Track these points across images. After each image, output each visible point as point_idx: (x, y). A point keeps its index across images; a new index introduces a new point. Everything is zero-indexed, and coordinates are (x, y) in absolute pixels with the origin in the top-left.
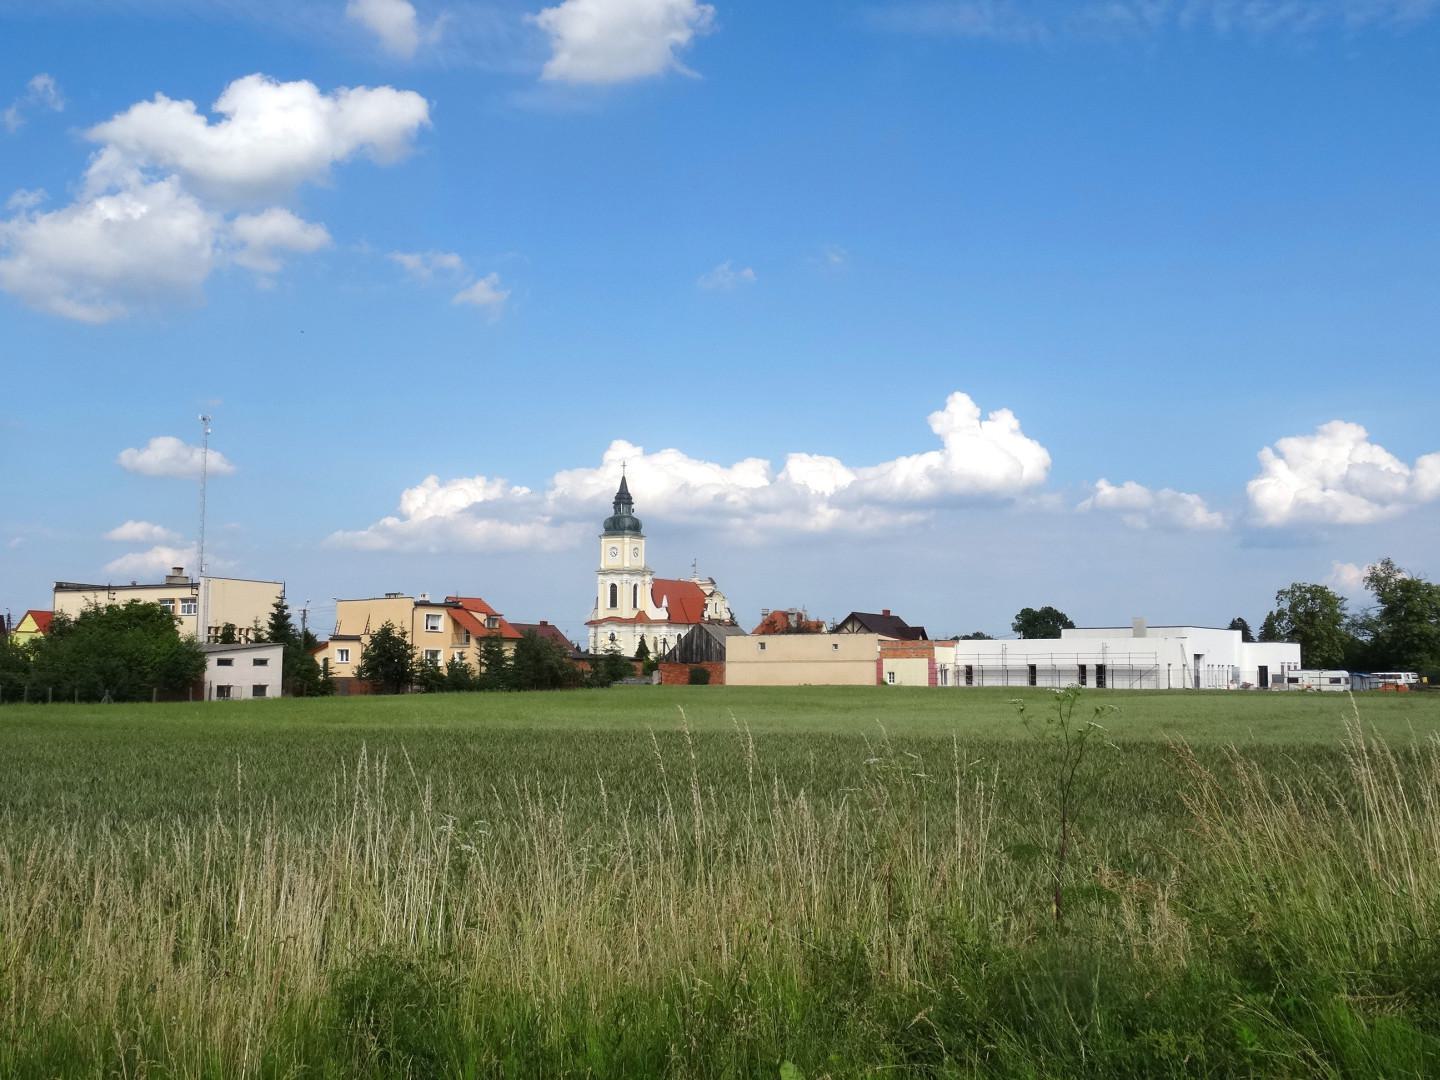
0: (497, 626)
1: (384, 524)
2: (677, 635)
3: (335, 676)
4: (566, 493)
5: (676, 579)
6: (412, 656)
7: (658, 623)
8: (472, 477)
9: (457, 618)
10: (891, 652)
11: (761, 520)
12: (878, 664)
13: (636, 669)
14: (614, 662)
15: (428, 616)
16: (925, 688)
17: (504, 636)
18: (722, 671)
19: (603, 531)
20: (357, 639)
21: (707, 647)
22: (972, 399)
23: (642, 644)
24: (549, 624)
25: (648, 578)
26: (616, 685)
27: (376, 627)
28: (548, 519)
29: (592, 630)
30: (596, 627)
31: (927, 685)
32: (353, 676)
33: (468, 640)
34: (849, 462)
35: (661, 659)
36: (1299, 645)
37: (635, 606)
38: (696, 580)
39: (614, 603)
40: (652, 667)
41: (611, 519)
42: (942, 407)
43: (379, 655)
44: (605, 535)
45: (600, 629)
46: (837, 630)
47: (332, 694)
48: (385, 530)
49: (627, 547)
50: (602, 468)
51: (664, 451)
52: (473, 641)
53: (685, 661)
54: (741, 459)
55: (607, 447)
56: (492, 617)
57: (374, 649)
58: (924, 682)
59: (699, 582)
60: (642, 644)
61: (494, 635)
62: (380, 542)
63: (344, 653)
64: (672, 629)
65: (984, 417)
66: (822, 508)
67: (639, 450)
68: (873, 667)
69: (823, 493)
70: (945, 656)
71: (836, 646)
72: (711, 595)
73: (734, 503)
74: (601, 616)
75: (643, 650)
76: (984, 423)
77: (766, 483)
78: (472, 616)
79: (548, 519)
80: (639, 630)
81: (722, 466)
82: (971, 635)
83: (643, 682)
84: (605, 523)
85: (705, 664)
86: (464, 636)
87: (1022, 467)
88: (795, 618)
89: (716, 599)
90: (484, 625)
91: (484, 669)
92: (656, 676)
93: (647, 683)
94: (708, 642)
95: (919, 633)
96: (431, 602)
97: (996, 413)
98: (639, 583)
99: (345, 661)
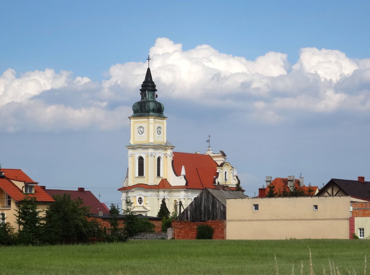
0: (33, 192)
4: (119, 83)
7: (178, 188)
8: (43, 70)
10: (361, 212)
11: (279, 103)
12: (350, 222)
13: (154, 227)
17: (38, 200)
19: (132, 113)
21: (213, 208)
23: (164, 205)
24: (85, 190)
25: (169, 152)
29: (124, 195)
33: (9, 204)
35: (175, 218)
36: (85, 190)
37: (159, 175)
38: (210, 153)
39: (141, 173)
40: (168, 225)
41: (139, 103)
44: (134, 117)
45: (130, 194)
46: (322, 192)
49: (151, 127)
51: (199, 47)
52: (13, 205)
53: (194, 220)
54: (263, 53)
56: (29, 184)
59: (212, 155)
60: (164, 205)
61: (30, 199)
64: (190, 194)
66: (330, 93)
68: (347, 223)
69: (331, 80)
71: (316, 207)
72: (222, 165)
73: (258, 89)
75: (164, 210)
77: (284, 72)
79: (105, 104)
80: (162, 194)
83: (159, 237)
84: (134, 106)
85: (210, 222)
86: (6, 200)
90: (22, 191)
91: (22, 227)
92: (170, 233)
93: (162, 238)
94: (214, 204)
98: (162, 156)
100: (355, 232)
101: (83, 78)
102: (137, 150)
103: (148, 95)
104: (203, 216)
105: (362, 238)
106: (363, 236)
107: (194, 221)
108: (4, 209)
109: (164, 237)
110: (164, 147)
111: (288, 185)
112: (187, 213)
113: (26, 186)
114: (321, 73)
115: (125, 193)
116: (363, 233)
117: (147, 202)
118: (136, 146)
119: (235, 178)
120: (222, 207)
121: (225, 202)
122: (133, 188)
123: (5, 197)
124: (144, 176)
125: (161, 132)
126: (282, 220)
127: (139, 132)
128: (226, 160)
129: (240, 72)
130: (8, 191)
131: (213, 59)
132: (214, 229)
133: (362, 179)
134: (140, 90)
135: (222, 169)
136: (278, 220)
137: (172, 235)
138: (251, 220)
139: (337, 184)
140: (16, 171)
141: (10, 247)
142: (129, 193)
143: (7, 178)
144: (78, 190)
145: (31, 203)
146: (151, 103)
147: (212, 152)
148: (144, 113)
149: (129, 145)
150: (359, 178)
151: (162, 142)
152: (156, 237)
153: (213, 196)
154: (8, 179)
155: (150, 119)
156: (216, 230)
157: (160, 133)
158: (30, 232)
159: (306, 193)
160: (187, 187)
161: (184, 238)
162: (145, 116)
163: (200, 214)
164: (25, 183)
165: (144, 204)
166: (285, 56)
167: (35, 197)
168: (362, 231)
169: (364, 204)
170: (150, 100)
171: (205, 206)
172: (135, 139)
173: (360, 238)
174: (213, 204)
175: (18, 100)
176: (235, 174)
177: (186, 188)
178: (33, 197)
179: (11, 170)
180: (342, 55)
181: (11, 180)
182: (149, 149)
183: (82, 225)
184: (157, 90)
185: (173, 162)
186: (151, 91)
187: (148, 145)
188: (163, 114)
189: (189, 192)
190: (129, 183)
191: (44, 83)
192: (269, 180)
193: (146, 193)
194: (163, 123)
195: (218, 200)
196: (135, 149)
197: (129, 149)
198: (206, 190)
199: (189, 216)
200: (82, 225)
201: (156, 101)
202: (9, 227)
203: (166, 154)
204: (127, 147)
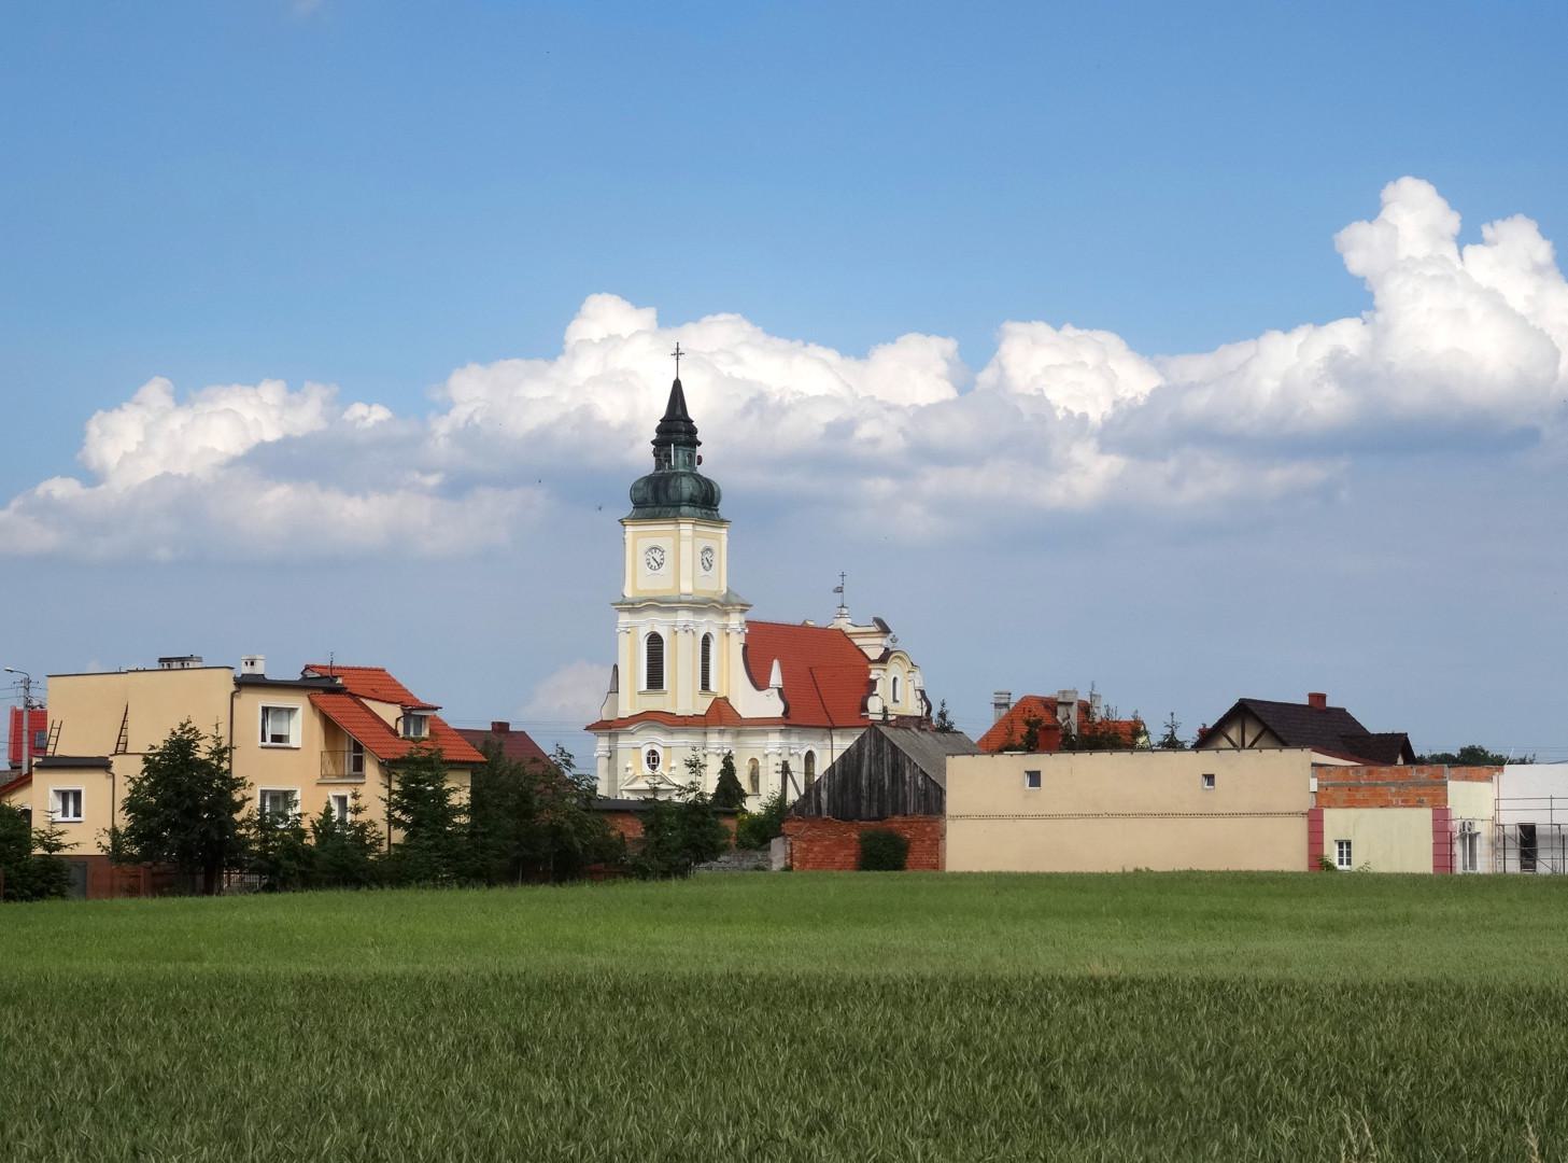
0: (426, 733)
1: (48, 494)
2: (803, 753)
3: (66, 852)
4: (477, 419)
5: (798, 622)
6: (239, 806)
8: (252, 381)
9: (333, 715)
10: (1342, 795)
11: (934, 481)
14: (699, 817)
15: (266, 710)
16: (1423, 876)
18: (938, 838)
20: (101, 765)
21: (894, 781)
22: (1441, 193)
25: (736, 621)
26: (702, 870)
27: (151, 735)
28: (432, 480)
29: (603, 743)
30: (613, 736)
31: (1431, 872)
32: (98, 852)
33: (358, 766)
34: (1147, 343)
35: (779, 812)
37: (705, 685)
38: (843, 624)
39: (655, 680)
41: (648, 480)
42: (1371, 210)
43: (166, 804)
45: (623, 741)
46: (1207, 739)
47: (61, 894)
48: (48, 510)
49: (686, 548)
50: (562, 360)
52: (371, 770)
55: (571, 309)
56: (415, 712)
57: (152, 791)
58: (1420, 861)
61: (425, 753)
62: (40, 538)
63: (70, 798)
64: (794, 740)
65: (1468, 236)
66: (1083, 453)
67: (648, 316)
68: (1300, 827)
70: (1470, 799)
71: (1210, 778)
72: (883, 659)
73: (874, 441)
74: (627, 707)
76: (1469, 250)
77: (947, 392)
78: (368, 710)
79: (432, 480)
81: (844, 352)
82: (1455, 753)
84: (635, 488)
87: (1556, 354)
88: (1074, 712)
89: (895, 668)
90: (395, 733)
92: (778, 852)
93: (757, 868)
94: (897, 770)
95: (1392, 749)
96: (268, 677)
97: (1498, 223)
98: (715, 632)
99: (71, 817)
100: (1326, 852)
101: (370, 406)
102: (645, 613)
103: (676, 456)
104: (864, 803)
105: (1345, 867)
106: (1349, 862)
107: (851, 820)
108: (344, 781)
109: (763, 864)
110: (722, 605)
111: (1058, 717)
112: (818, 794)
113: (407, 715)
114: (1057, 395)
115: (607, 738)
116: (1349, 854)
117: (673, 765)
118: (640, 603)
119: (918, 693)
120: (920, 778)
121: (942, 769)
122: (631, 724)
123: (346, 749)
124: (665, 688)
125: (713, 564)
126: (1110, 815)
127: (649, 564)
128: (896, 644)
129: (822, 393)
130: (358, 730)
131: (746, 353)
132: (909, 841)
133: (1320, 699)
134: (653, 442)
135: (885, 670)
136: (1097, 816)
137: (786, 858)
138: (1019, 817)
139: (1256, 712)
140: (371, 673)
141: (339, 891)
142: (620, 738)
143: (350, 693)
144: (490, 729)
145: (429, 766)
146: (684, 479)
147: (849, 621)
148: (664, 509)
149: (620, 599)
150: (1311, 696)
151: (716, 592)
152: (736, 864)
153: (894, 747)
154: (352, 695)
155: (682, 526)
156: (916, 846)
157: (711, 566)
158: (429, 849)
159: (1126, 739)
160: (788, 722)
161: (819, 865)
162: (666, 517)
163: (858, 798)
164: (403, 707)
165: (664, 769)
166: (950, 345)
167: (440, 750)
168: (1345, 849)
169: (1351, 772)
170: (681, 470)
171: (870, 775)
172: (639, 581)
173: (1340, 867)
174: (893, 771)
175: (182, 468)
176: (919, 683)
177: (786, 725)
178: (432, 747)
179: (359, 669)
180: (1111, 340)
181: (363, 700)
182: (680, 612)
183: (572, 828)
184: (700, 444)
185: (745, 648)
186: (684, 445)
187: (676, 599)
188: (717, 510)
189: (793, 735)
190: (621, 708)
191: (256, 419)
192: (1003, 701)
193: (670, 737)
194: (717, 538)
195: (910, 760)
196: (639, 610)
197: (621, 610)
198: (873, 730)
199: (824, 806)
200: (572, 828)
201: (699, 475)
202: (374, 835)
203: (726, 626)
204: (613, 604)
